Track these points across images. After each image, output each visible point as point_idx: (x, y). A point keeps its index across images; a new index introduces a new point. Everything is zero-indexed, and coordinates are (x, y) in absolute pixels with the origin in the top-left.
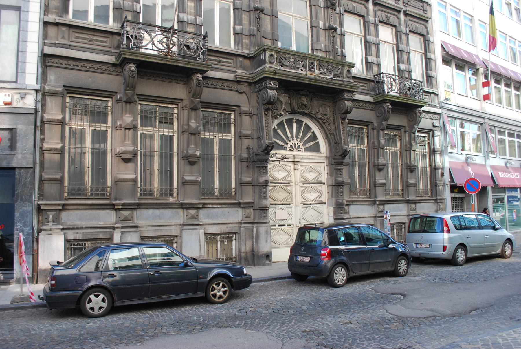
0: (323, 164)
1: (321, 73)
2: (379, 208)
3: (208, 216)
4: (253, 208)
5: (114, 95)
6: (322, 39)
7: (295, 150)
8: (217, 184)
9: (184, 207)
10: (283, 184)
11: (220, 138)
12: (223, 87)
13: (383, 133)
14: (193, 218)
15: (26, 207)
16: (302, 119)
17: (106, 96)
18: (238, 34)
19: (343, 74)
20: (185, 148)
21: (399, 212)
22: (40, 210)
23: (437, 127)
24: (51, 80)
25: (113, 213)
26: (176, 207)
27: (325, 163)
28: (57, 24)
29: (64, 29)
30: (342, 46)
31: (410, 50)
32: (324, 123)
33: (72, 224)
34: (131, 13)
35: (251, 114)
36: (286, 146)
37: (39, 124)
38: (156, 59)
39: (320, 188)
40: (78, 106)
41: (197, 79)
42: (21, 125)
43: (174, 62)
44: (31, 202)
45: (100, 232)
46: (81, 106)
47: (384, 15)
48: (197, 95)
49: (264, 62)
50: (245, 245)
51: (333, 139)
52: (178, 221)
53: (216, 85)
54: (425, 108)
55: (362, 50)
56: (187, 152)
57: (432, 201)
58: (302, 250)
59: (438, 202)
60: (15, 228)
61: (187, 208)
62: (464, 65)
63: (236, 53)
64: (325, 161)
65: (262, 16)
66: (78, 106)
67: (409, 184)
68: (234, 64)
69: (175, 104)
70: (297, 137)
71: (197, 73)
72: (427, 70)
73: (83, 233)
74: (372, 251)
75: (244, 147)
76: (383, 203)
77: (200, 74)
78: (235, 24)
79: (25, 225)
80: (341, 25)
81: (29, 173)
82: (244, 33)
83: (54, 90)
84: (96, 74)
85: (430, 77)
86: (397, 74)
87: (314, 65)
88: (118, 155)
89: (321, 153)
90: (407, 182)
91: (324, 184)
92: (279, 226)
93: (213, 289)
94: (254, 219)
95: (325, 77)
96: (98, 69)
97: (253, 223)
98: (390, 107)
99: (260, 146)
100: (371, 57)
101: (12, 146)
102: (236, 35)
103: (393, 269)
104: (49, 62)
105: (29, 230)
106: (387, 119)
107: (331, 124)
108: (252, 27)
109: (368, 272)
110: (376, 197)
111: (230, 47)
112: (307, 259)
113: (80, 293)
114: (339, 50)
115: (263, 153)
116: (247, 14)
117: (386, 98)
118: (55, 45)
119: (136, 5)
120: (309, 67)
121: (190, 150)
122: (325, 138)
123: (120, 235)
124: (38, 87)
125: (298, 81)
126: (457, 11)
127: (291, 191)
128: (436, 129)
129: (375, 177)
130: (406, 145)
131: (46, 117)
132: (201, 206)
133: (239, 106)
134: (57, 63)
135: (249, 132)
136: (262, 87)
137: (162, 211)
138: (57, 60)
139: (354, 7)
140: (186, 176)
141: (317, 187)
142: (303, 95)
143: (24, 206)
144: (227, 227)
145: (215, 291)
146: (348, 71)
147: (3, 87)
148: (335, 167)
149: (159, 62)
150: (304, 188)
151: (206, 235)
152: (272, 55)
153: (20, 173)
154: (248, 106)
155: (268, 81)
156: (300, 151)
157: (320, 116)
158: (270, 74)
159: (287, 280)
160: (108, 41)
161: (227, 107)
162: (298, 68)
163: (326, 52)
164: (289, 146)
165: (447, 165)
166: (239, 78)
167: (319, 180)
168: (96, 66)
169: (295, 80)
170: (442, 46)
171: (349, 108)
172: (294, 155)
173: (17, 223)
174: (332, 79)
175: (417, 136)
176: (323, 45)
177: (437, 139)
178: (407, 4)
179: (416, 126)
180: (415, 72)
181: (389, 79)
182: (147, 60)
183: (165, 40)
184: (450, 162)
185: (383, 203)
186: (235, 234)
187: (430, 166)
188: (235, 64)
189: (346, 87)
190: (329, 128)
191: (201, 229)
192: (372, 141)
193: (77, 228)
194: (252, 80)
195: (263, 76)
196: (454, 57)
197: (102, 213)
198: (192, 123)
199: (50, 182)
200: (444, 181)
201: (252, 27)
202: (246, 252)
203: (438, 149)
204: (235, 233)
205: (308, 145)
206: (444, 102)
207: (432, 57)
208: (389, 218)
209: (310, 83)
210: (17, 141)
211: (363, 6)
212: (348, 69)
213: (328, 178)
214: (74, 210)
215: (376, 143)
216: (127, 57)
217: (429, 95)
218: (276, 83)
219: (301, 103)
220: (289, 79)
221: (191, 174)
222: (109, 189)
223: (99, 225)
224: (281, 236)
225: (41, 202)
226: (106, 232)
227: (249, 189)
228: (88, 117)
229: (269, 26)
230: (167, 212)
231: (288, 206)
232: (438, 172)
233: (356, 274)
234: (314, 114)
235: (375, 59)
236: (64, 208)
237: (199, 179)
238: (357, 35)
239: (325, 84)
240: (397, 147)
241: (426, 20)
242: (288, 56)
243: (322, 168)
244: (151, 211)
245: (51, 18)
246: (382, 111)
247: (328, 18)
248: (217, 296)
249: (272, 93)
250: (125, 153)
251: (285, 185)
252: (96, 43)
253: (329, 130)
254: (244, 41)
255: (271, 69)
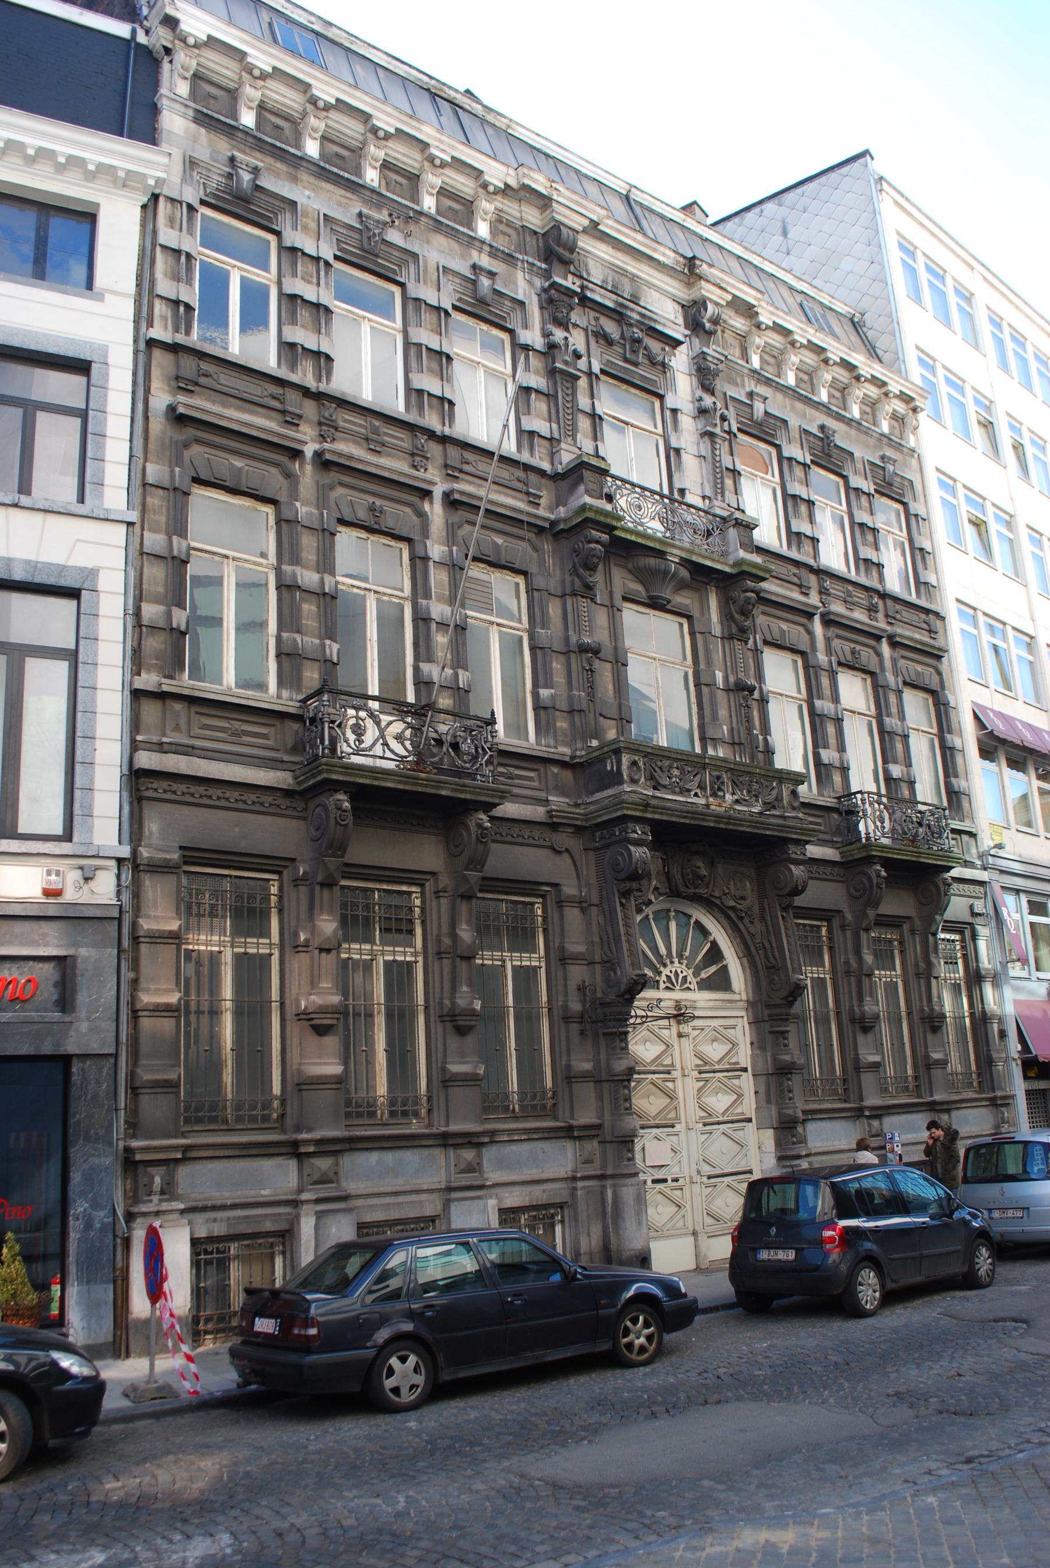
0: (740, 1020)
1: (737, 801)
2: (869, 1125)
3: (501, 1164)
4: (600, 1139)
5: (286, 867)
6: (723, 712)
7: (678, 988)
8: (514, 1084)
9: (451, 1142)
10: (657, 1076)
11: (516, 963)
12: (520, 840)
13: (868, 935)
14: (470, 1169)
15: (99, 1156)
16: (689, 911)
17: (264, 867)
18: (545, 708)
19: (781, 800)
20: (446, 994)
21: (914, 1135)
22: (130, 1163)
23: (980, 915)
24: (151, 833)
25: (292, 1164)
26: (430, 1142)
27: (745, 1018)
28: (162, 696)
29: (178, 706)
30: (766, 729)
31: (908, 728)
32: (741, 919)
33: (201, 1196)
34: (318, 663)
35: (584, 905)
36: (658, 978)
37: (126, 943)
38: (394, 781)
39: (736, 1082)
40: (207, 896)
41: (480, 826)
42: (87, 947)
43: (433, 787)
44: (110, 1144)
45: (266, 1215)
46: (215, 894)
47: (847, 647)
48: (478, 862)
49: (616, 778)
50: (589, 1235)
51: (762, 956)
52: (435, 1180)
53: (518, 836)
54: (955, 872)
55: (804, 733)
56: (453, 1003)
57: (984, 1103)
58: (773, 1234)
59: (999, 1103)
60: (72, 1212)
61: (456, 1146)
62: (1025, 758)
63: (545, 755)
64: (743, 1013)
65: (597, 663)
66: (207, 896)
67: (931, 1061)
68: (540, 783)
69: (416, 884)
70: (680, 956)
71: (477, 811)
72: (947, 775)
73: (228, 1219)
74: (922, 1228)
75: (572, 986)
76: (879, 1112)
77: (484, 812)
78: (536, 685)
79: (95, 1205)
80: (760, 676)
81: (105, 1070)
82: (557, 707)
83: (160, 859)
84: (250, 815)
85: (956, 793)
86: (883, 791)
87: (723, 783)
88: (303, 1016)
89: (733, 992)
90: (927, 1056)
91: (745, 1070)
92: (655, 1181)
93: (627, 1332)
94: (604, 1165)
95: (745, 809)
96: (254, 803)
97: (602, 1177)
98: (883, 874)
99: (608, 982)
100: (827, 751)
101: (65, 1002)
102: (542, 712)
103: (965, 1269)
104: (147, 789)
105: (105, 1217)
106: (876, 904)
107: (757, 921)
108: (575, 692)
109: (919, 1279)
110: (861, 1099)
111: (527, 740)
112: (791, 1255)
113: (372, 1352)
114: (761, 738)
115: (620, 999)
116: (562, 658)
117: (874, 853)
118: (160, 748)
119: (330, 646)
120: (712, 788)
121: (461, 998)
122: (741, 955)
123: (314, 1222)
124: (125, 851)
125: (693, 822)
126: (996, 625)
127: (674, 1091)
128: (979, 920)
129: (856, 1049)
130: (917, 965)
131: (146, 925)
132: (486, 1140)
133: (555, 885)
134: (165, 791)
135: (581, 949)
136: (613, 839)
137: (399, 1154)
138: (164, 784)
139: (782, 631)
140: (452, 1063)
141: (730, 1078)
142: (696, 853)
143: (93, 1155)
144: (544, 1191)
145: (632, 1336)
146: (794, 793)
147: (42, 852)
148: (772, 1027)
149: (401, 787)
150: (702, 1083)
151: (501, 1211)
152: (634, 763)
153: (83, 1069)
154: (576, 883)
155: (631, 825)
156: (689, 989)
157: (732, 903)
158: (635, 810)
159: (722, 1313)
160: (272, 734)
161: (529, 887)
162: (689, 791)
163: (733, 744)
164: (664, 978)
165: (1010, 1010)
166: (557, 816)
167: (733, 1060)
168: (250, 797)
169: (688, 821)
170: (976, 716)
171: (800, 882)
172: (677, 1001)
173: (75, 1201)
174: (761, 813)
175: (943, 940)
176: (725, 728)
177: (982, 945)
178: (895, 618)
179: (938, 917)
180: (922, 783)
181: (876, 806)
182: (376, 783)
183: (408, 733)
184: (1016, 1002)
185: (880, 1112)
186: (562, 1208)
187: (972, 1015)
188: (543, 784)
189: (792, 833)
190: (752, 930)
191: (491, 1198)
192: (843, 957)
193: (214, 1208)
194: (586, 820)
195: (619, 813)
196: (1004, 742)
197: (267, 1165)
198: (464, 930)
199: (153, 1090)
200: (1006, 1049)
201: (575, 692)
202: (591, 1254)
203: (986, 969)
204: (561, 1206)
205: (704, 975)
206: (992, 852)
207: (957, 743)
208: (898, 1150)
209: (717, 825)
210: (78, 988)
211: (801, 629)
212: (792, 787)
213: (753, 1056)
214: (205, 1162)
215: (854, 964)
216: (334, 777)
217: (958, 837)
218: (648, 829)
219: (692, 871)
220: (674, 819)
221: (462, 1059)
222: (276, 1104)
223: (262, 1196)
224: (660, 1208)
225: (135, 1144)
226: (279, 1214)
227: (586, 1092)
228: (225, 923)
229: (610, 687)
230: (411, 1157)
231: (670, 1129)
232: (992, 1029)
233: (898, 1285)
234: (719, 898)
235: (837, 755)
236: (188, 1156)
237: (481, 1071)
238: (792, 697)
239: (748, 826)
240: (895, 969)
241: (935, 655)
242: (667, 763)
243: (739, 1029)
244: (374, 1157)
245: (148, 680)
246: (863, 883)
247: (731, 664)
248: (636, 1348)
249: (639, 852)
250: (323, 1010)
251: (662, 1076)
252: (245, 739)
253: (752, 935)
254: (559, 724)
255: (635, 798)
